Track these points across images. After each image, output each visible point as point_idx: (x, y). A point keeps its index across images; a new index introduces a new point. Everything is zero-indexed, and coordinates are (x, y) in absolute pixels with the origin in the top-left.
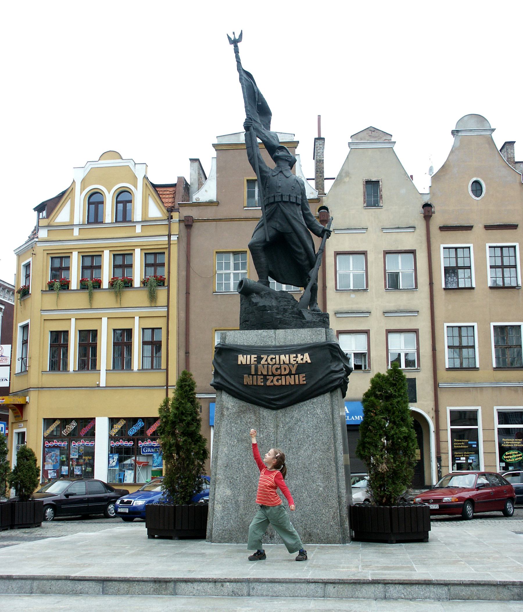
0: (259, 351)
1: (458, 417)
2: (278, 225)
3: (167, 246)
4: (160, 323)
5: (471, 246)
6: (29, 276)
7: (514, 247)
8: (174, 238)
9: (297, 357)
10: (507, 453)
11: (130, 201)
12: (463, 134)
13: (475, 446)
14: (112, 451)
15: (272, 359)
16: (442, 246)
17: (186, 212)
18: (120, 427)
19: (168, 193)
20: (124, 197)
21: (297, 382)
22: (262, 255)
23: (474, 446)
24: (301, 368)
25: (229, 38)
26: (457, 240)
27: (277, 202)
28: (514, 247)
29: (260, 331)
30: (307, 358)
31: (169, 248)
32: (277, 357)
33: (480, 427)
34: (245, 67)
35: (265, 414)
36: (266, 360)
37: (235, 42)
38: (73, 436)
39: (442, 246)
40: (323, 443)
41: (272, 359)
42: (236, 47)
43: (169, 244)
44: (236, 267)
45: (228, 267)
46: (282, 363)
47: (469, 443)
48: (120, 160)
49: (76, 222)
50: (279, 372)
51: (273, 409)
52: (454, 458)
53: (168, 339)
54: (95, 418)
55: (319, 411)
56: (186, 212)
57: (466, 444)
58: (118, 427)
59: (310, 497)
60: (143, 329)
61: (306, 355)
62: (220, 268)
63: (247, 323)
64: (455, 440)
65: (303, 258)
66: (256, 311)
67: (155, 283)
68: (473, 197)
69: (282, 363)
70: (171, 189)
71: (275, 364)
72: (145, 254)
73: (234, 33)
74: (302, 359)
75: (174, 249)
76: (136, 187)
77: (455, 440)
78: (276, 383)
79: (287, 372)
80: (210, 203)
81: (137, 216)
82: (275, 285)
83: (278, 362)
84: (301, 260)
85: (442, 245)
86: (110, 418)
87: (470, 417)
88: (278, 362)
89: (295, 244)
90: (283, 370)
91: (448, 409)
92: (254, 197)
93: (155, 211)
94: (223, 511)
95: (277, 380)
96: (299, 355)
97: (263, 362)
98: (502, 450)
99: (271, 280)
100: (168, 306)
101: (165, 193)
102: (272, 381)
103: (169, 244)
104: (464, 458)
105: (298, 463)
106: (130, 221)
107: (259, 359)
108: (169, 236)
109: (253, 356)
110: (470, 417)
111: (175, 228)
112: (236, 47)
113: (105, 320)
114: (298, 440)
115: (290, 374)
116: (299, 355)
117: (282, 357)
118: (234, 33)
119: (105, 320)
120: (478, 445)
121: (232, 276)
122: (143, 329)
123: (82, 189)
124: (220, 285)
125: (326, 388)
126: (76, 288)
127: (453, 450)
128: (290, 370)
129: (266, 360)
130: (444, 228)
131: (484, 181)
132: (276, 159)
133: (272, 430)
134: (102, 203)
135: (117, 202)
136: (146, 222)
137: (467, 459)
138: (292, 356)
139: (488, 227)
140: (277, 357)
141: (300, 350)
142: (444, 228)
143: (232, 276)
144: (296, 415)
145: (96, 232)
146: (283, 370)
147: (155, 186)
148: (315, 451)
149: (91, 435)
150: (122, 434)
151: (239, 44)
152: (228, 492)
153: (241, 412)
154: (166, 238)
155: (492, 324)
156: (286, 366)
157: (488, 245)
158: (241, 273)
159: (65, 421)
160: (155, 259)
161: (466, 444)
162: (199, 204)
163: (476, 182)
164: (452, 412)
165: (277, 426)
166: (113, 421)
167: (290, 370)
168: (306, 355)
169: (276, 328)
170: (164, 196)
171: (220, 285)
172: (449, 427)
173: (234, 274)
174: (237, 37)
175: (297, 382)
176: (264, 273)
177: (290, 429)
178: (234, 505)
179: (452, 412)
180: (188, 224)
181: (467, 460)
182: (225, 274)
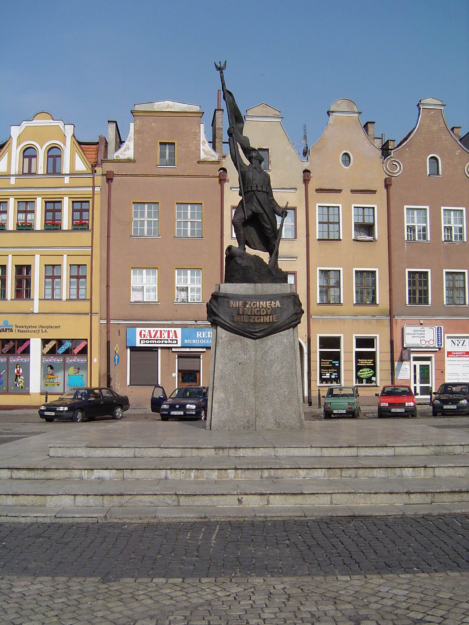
0: (245, 298)
1: (325, 342)
2: (254, 207)
3: (91, 196)
4: (86, 260)
5: (340, 205)
6: (321, 292)
7: (373, 208)
8: (97, 189)
9: (271, 303)
10: (361, 371)
11: (60, 156)
12: (337, 114)
13: (337, 365)
14: (43, 365)
15: (254, 304)
16: (318, 205)
17: (108, 167)
18: (51, 347)
19: (91, 150)
20: (54, 152)
21: (271, 321)
22: (241, 228)
23: (337, 365)
24: (274, 311)
25: (216, 66)
26: (329, 201)
27: (254, 191)
28: (373, 208)
29: (244, 284)
30: (278, 303)
31: (93, 197)
32: (258, 303)
33: (342, 350)
34: (228, 88)
35: (248, 342)
36: (250, 305)
37: (220, 69)
38: (12, 352)
39: (318, 205)
40: (288, 362)
41: (254, 304)
42: (222, 72)
43: (94, 194)
44: (149, 216)
45: (142, 215)
46: (261, 307)
47: (333, 362)
48: (52, 121)
49: (12, 173)
50: (259, 313)
51: (255, 339)
52: (321, 375)
53: (91, 274)
54: (29, 339)
55: (285, 340)
56: (108, 167)
57: (331, 363)
58: (49, 346)
59: (279, 398)
60: (70, 265)
61: (278, 302)
62: (136, 216)
63: (229, 278)
64: (322, 360)
65: (270, 232)
66: (235, 268)
67: (80, 225)
68: (343, 166)
69: (261, 307)
70: (95, 146)
71: (256, 308)
72: (73, 202)
73: (220, 63)
74: (275, 305)
75: (97, 198)
76: (65, 144)
77: (322, 360)
78: (256, 321)
79: (265, 313)
80: (129, 161)
81: (66, 169)
82: (249, 251)
83: (258, 306)
84: (268, 233)
85: (318, 203)
86: (42, 339)
87: (335, 342)
88: (258, 306)
89: (265, 222)
90: (262, 312)
91: (318, 335)
92: (165, 157)
93: (81, 166)
94: (219, 408)
95: (258, 319)
96: (273, 302)
97: (247, 306)
98: (358, 368)
99: (246, 246)
100: (92, 247)
101: (89, 150)
102: (254, 319)
103: (94, 194)
104: (329, 374)
105: (270, 376)
106: (60, 174)
107: (245, 304)
108: (94, 187)
109: (240, 302)
110: (335, 342)
111: (99, 180)
112: (222, 72)
113: (37, 257)
114: (271, 360)
115: (266, 315)
116: (273, 302)
117: (261, 302)
118: (220, 63)
119: (37, 257)
120: (339, 363)
121: (146, 223)
122: (70, 265)
123: (18, 144)
124: (136, 230)
125: (291, 325)
126: (12, 229)
127: (321, 368)
128: (267, 312)
129: (250, 305)
130: (318, 190)
131: (352, 154)
132: (250, 159)
133: (253, 353)
134: (35, 156)
135: (48, 157)
136: (72, 174)
137: (331, 374)
138: (268, 302)
139: (352, 191)
140: (258, 303)
141: (271, 298)
142: (318, 190)
143: (146, 223)
144: (270, 343)
145: (28, 181)
146: (262, 312)
147: (80, 144)
148: (282, 368)
149: (27, 351)
150: (52, 352)
151: (224, 71)
152: (222, 395)
153: (231, 341)
154: (91, 189)
155: (355, 269)
156: (264, 309)
157: (353, 206)
158: (154, 221)
159: (60, 342)
160: (81, 206)
161: (331, 363)
162: (119, 161)
163: (346, 154)
164: (321, 338)
165: (256, 351)
166: (45, 342)
167: (267, 312)
168: (278, 302)
169: (255, 282)
170: (88, 152)
171: (136, 230)
172: (319, 350)
173: (148, 221)
174: (222, 66)
175: (271, 321)
176: (243, 241)
177: (266, 352)
178: (226, 404)
179: (321, 338)
180: (109, 178)
181: (330, 376)
182: (141, 221)
